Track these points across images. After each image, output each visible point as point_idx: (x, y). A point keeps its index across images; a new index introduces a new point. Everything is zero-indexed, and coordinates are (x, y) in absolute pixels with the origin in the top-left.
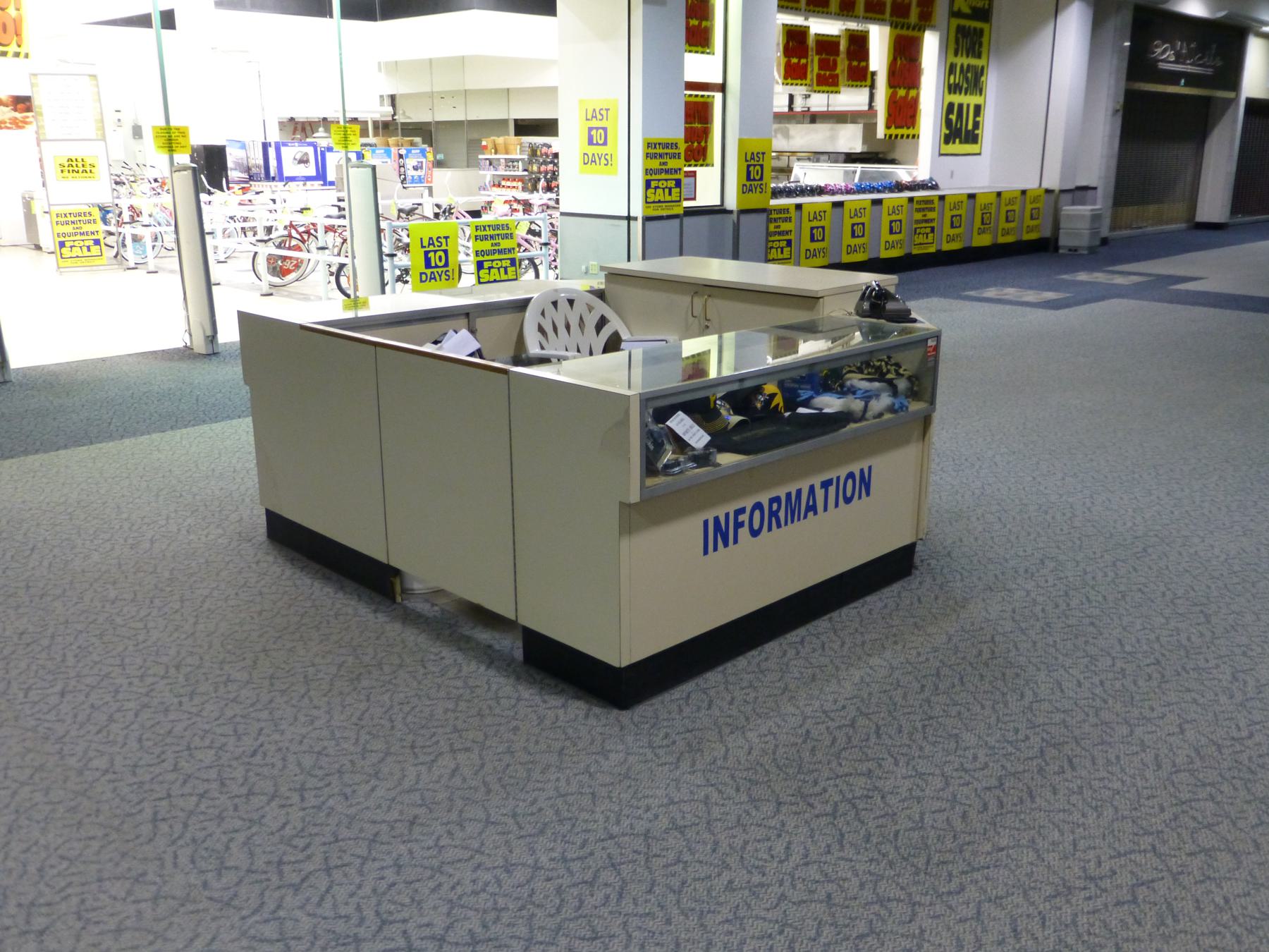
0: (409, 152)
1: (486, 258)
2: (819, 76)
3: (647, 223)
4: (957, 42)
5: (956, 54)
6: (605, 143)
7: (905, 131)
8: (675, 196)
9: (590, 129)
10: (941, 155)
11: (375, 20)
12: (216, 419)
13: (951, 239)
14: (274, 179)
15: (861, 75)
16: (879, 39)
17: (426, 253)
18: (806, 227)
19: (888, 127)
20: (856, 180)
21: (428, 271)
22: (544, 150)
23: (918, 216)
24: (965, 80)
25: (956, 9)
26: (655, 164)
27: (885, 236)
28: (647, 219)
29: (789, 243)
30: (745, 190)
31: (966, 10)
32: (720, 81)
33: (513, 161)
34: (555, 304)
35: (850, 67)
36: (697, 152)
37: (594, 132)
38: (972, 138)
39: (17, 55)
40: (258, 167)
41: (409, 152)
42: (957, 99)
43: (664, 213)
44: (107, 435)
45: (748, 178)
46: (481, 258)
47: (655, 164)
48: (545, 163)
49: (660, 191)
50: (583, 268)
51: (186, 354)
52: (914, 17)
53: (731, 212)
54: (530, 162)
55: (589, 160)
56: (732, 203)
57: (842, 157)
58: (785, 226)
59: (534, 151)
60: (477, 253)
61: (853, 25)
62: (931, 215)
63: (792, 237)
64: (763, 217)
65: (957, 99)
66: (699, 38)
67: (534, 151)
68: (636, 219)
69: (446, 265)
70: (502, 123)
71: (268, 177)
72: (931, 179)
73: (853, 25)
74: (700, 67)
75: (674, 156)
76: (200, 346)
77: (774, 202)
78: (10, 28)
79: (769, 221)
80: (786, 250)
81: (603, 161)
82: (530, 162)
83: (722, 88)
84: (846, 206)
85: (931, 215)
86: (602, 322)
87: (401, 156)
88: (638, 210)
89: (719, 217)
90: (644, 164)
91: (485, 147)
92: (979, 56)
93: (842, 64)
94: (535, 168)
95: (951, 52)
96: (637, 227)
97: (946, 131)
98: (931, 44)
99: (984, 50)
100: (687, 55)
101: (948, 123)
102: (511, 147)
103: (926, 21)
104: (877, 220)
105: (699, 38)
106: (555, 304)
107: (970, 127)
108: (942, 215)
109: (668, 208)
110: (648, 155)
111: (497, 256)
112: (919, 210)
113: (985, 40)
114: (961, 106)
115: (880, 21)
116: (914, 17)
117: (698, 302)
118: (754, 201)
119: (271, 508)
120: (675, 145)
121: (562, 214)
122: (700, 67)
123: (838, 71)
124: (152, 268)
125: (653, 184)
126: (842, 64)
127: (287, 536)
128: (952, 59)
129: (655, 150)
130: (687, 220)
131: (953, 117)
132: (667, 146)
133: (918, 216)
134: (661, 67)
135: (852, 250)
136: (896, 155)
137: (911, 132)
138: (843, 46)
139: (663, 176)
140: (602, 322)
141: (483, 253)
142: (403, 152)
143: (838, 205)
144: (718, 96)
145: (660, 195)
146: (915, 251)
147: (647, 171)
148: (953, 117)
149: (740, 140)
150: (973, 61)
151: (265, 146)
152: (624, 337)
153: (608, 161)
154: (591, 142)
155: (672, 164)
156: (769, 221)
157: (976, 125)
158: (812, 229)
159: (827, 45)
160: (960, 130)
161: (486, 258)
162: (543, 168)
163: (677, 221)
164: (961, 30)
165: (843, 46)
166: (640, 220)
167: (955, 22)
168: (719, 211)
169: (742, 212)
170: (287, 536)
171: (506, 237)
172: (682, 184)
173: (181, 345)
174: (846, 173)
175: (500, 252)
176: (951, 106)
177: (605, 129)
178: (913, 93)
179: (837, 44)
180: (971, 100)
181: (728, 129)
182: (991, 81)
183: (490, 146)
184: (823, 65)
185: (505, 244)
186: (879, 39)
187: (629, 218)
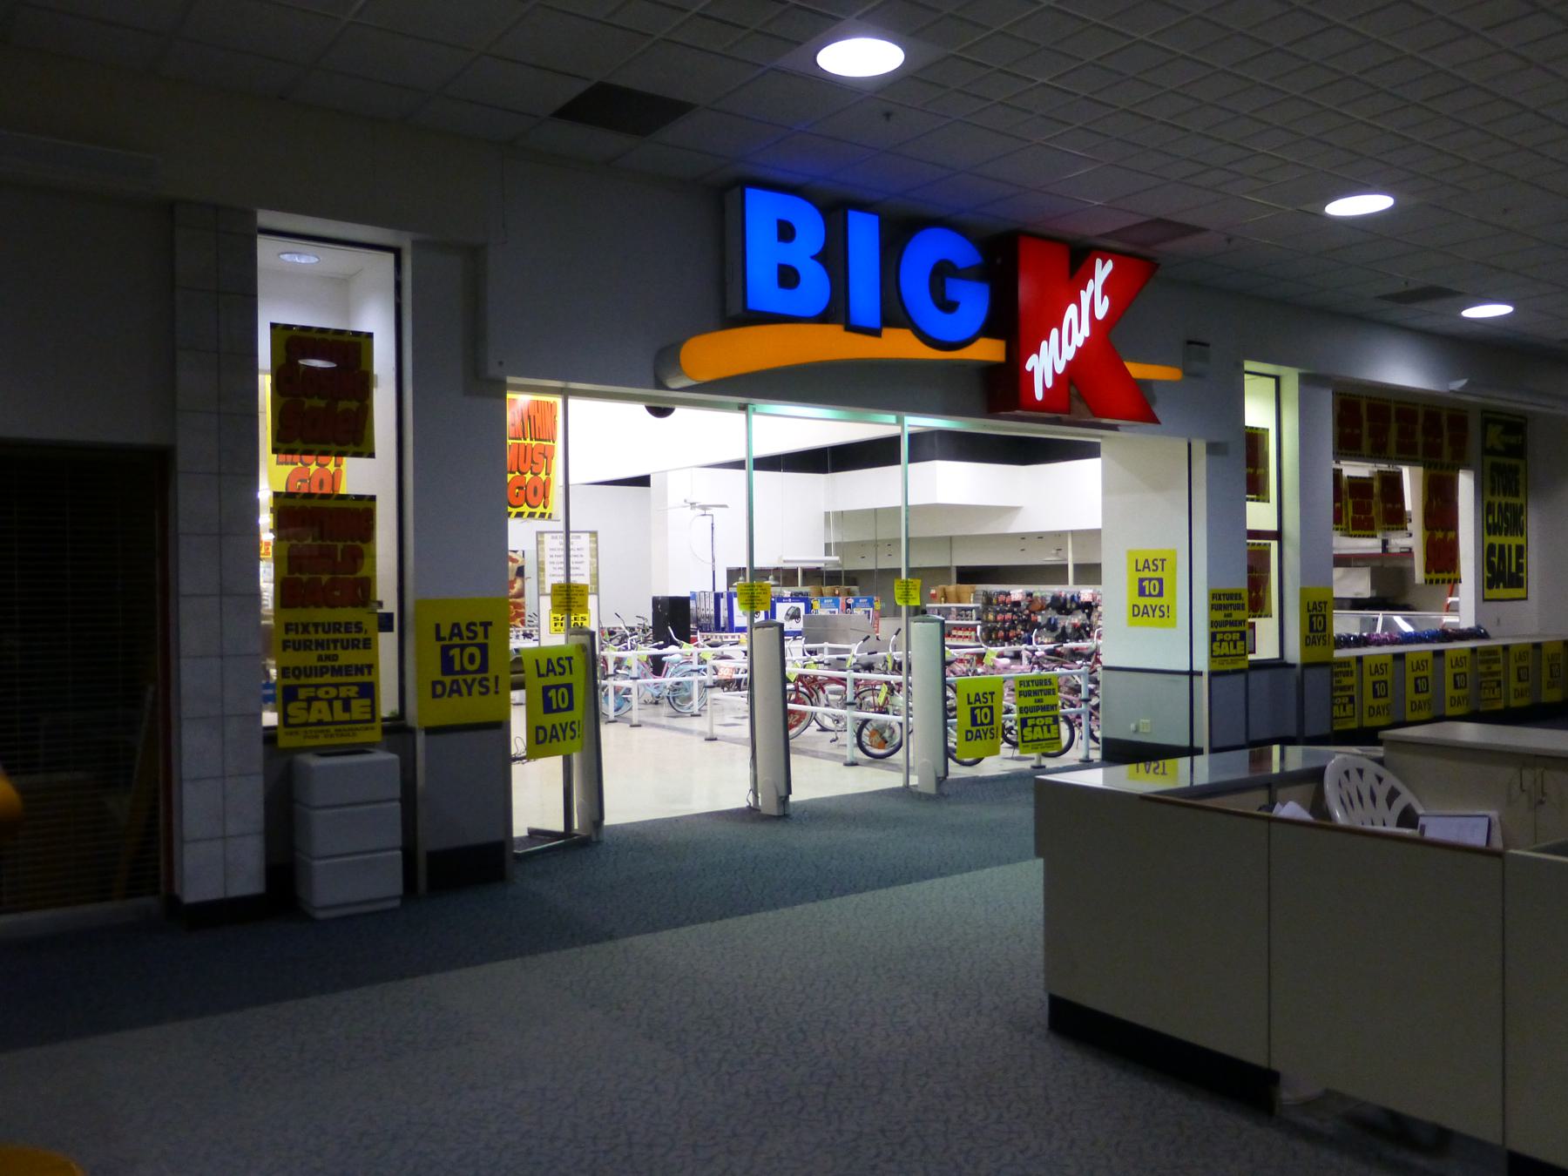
0: (857, 600)
1: (303, 680)
2: (1353, 520)
3: (1218, 681)
4: (1493, 481)
5: (1492, 493)
6: (1160, 594)
7: (1446, 576)
8: (1240, 650)
9: (1141, 581)
10: (1485, 600)
11: (825, 471)
12: (845, 892)
13: (1519, 694)
14: (723, 630)
15: (1397, 518)
16: (1411, 480)
17: (973, 710)
18: (1368, 680)
19: (1427, 571)
20: (1379, 630)
21: (974, 729)
22: (1002, 598)
23: (1482, 668)
24: (1501, 519)
25: (1488, 445)
26: (1220, 616)
27: (1450, 691)
28: (1213, 674)
29: (1351, 699)
30: (1307, 641)
31: (1500, 447)
32: (1275, 528)
33: (966, 609)
34: (1347, 773)
35: (1385, 509)
36: (1258, 606)
37: (1146, 583)
38: (1516, 581)
39: (542, 515)
40: (709, 617)
41: (857, 600)
42: (1497, 540)
43: (1230, 667)
44: (747, 906)
45: (1311, 630)
46: (291, 681)
47: (1220, 616)
48: (1004, 612)
49: (1225, 644)
50: (1133, 726)
51: (750, 815)
52: (1447, 455)
53: (1293, 666)
54: (986, 611)
55: (1138, 612)
56: (1294, 654)
57: (1346, 604)
58: (1347, 681)
59: (988, 600)
60: (1021, 710)
61: (1384, 467)
62: (1495, 667)
63: (1355, 693)
64: (1326, 672)
65: (1497, 540)
66: (1256, 488)
67: (988, 600)
68: (1200, 674)
69: (991, 722)
70: (945, 570)
71: (718, 629)
72: (1479, 627)
73: (1384, 467)
74: (1260, 515)
75: (1239, 607)
76: (768, 805)
77: (1339, 654)
78: (540, 491)
79: (1333, 674)
80: (1349, 707)
81: (1158, 613)
82: (986, 611)
83: (1278, 535)
84: (1408, 658)
85: (1495, 667)
86: (1393, 795)
87: (848, 606)
88: (1202, 663)
89: (1281, 671)
90: (1209, 616)
91: (934, 596)
92: (1516, 494)
93: (1377, 508)
94: (991, 617)
95: (1487, 493)
96: (1202, 684)
97: (1487, 574)
98: (1466, 484)
99: (1522, 489)
100: (1249, 504)
101: (1490, 566)
102: (964, 596)
103: (1460, 462)
104: (1440, 672)
105: (1256, 488)
106: (1347, 773)
107: (1514, 569)
108: (1507, 666)
109: (1233, 662)
110: (1213, 607)
111: (1040, 713)
112: (1482, 662)
113: (1521, 477)
114: (1502, 547)
115: (1411, 462)
116: (1447, 455)
117: (1528, 775)
118: (1318, 653)
119: (1059, 993)
120: (1238, 596)
121: (1105, 668)
122: (1260, 515)
123: (1373, 513)
124: (635, 722)
125: (1219, 637)
126: (1377, 508)
127: (1072, 1022)
128: (1488, 498)
129: (1218, 601)
130: (1253, 675)
131: (1495, 560)
132: (1230, 596)
133: (1482, 668)
134: (1226, 517)
135: (1417, 707)
136: (1410, 600)
137: (1452, 576)
138: (1376, 485)
139: (1228, 628)
140: (1393, 795)
141: (298, 672)
142: (851, 601)
143: (1399, 657)
144: (1274, 544)
145: (1225, 649)
146: (1482, 709)
147: (1213, 624)
148: (1495, 560)
149: (1302, 590)
150: (1511, 500)
151: (718, 597)
152: (1420, 811)
153: (1164, 613)
154: (1142, 592)
155: (1237, 615)
156: (1333, 674)
157: (1520, 567)
158: (1374, 683)
159: (1359, 487)
160: (1501, 574)
161: (303, 680)
162: (1000, 617)
163: (1242, 677)
164: (1495, 468)
165: (1376, 485)
166: (1205, 677)
167: (1489, 459)
168: (1279, 665)
169: (1306, 666)
170: (1072, 1022)
171: (1048, 692)
172: (1246, 637)
173: (744, 804)
174: (1363, 621)
175: (337, 671)
176: (1491, 547)
177: (1161, 581)
178: (1451, 535)
179: (1371, 487)
180: (1513, 541)
181: (1287, 578)
182: (1533, 521)
183: (940, 594)
184: (1358, 508)
185: (1048, 700)
186: (1411, 480)
187: (1192, 673)
